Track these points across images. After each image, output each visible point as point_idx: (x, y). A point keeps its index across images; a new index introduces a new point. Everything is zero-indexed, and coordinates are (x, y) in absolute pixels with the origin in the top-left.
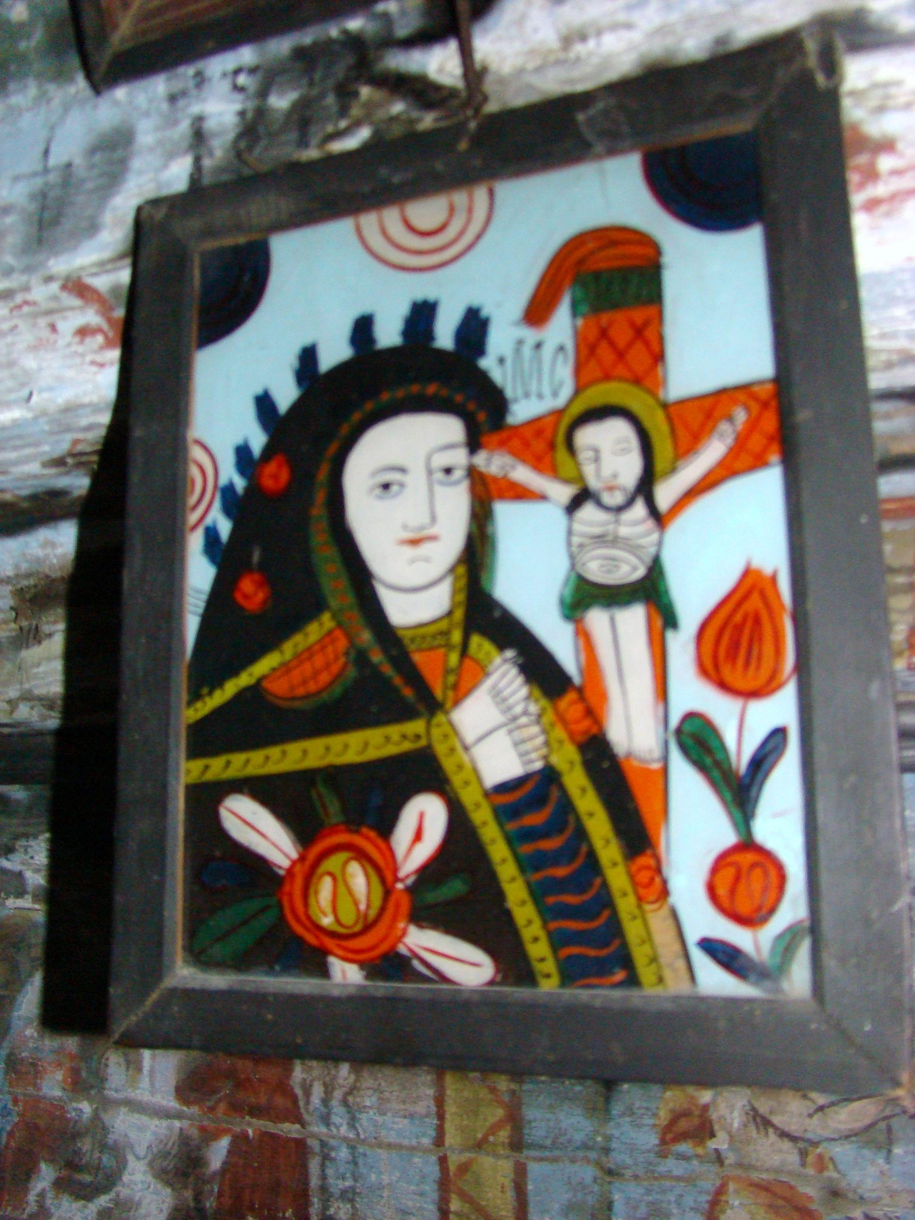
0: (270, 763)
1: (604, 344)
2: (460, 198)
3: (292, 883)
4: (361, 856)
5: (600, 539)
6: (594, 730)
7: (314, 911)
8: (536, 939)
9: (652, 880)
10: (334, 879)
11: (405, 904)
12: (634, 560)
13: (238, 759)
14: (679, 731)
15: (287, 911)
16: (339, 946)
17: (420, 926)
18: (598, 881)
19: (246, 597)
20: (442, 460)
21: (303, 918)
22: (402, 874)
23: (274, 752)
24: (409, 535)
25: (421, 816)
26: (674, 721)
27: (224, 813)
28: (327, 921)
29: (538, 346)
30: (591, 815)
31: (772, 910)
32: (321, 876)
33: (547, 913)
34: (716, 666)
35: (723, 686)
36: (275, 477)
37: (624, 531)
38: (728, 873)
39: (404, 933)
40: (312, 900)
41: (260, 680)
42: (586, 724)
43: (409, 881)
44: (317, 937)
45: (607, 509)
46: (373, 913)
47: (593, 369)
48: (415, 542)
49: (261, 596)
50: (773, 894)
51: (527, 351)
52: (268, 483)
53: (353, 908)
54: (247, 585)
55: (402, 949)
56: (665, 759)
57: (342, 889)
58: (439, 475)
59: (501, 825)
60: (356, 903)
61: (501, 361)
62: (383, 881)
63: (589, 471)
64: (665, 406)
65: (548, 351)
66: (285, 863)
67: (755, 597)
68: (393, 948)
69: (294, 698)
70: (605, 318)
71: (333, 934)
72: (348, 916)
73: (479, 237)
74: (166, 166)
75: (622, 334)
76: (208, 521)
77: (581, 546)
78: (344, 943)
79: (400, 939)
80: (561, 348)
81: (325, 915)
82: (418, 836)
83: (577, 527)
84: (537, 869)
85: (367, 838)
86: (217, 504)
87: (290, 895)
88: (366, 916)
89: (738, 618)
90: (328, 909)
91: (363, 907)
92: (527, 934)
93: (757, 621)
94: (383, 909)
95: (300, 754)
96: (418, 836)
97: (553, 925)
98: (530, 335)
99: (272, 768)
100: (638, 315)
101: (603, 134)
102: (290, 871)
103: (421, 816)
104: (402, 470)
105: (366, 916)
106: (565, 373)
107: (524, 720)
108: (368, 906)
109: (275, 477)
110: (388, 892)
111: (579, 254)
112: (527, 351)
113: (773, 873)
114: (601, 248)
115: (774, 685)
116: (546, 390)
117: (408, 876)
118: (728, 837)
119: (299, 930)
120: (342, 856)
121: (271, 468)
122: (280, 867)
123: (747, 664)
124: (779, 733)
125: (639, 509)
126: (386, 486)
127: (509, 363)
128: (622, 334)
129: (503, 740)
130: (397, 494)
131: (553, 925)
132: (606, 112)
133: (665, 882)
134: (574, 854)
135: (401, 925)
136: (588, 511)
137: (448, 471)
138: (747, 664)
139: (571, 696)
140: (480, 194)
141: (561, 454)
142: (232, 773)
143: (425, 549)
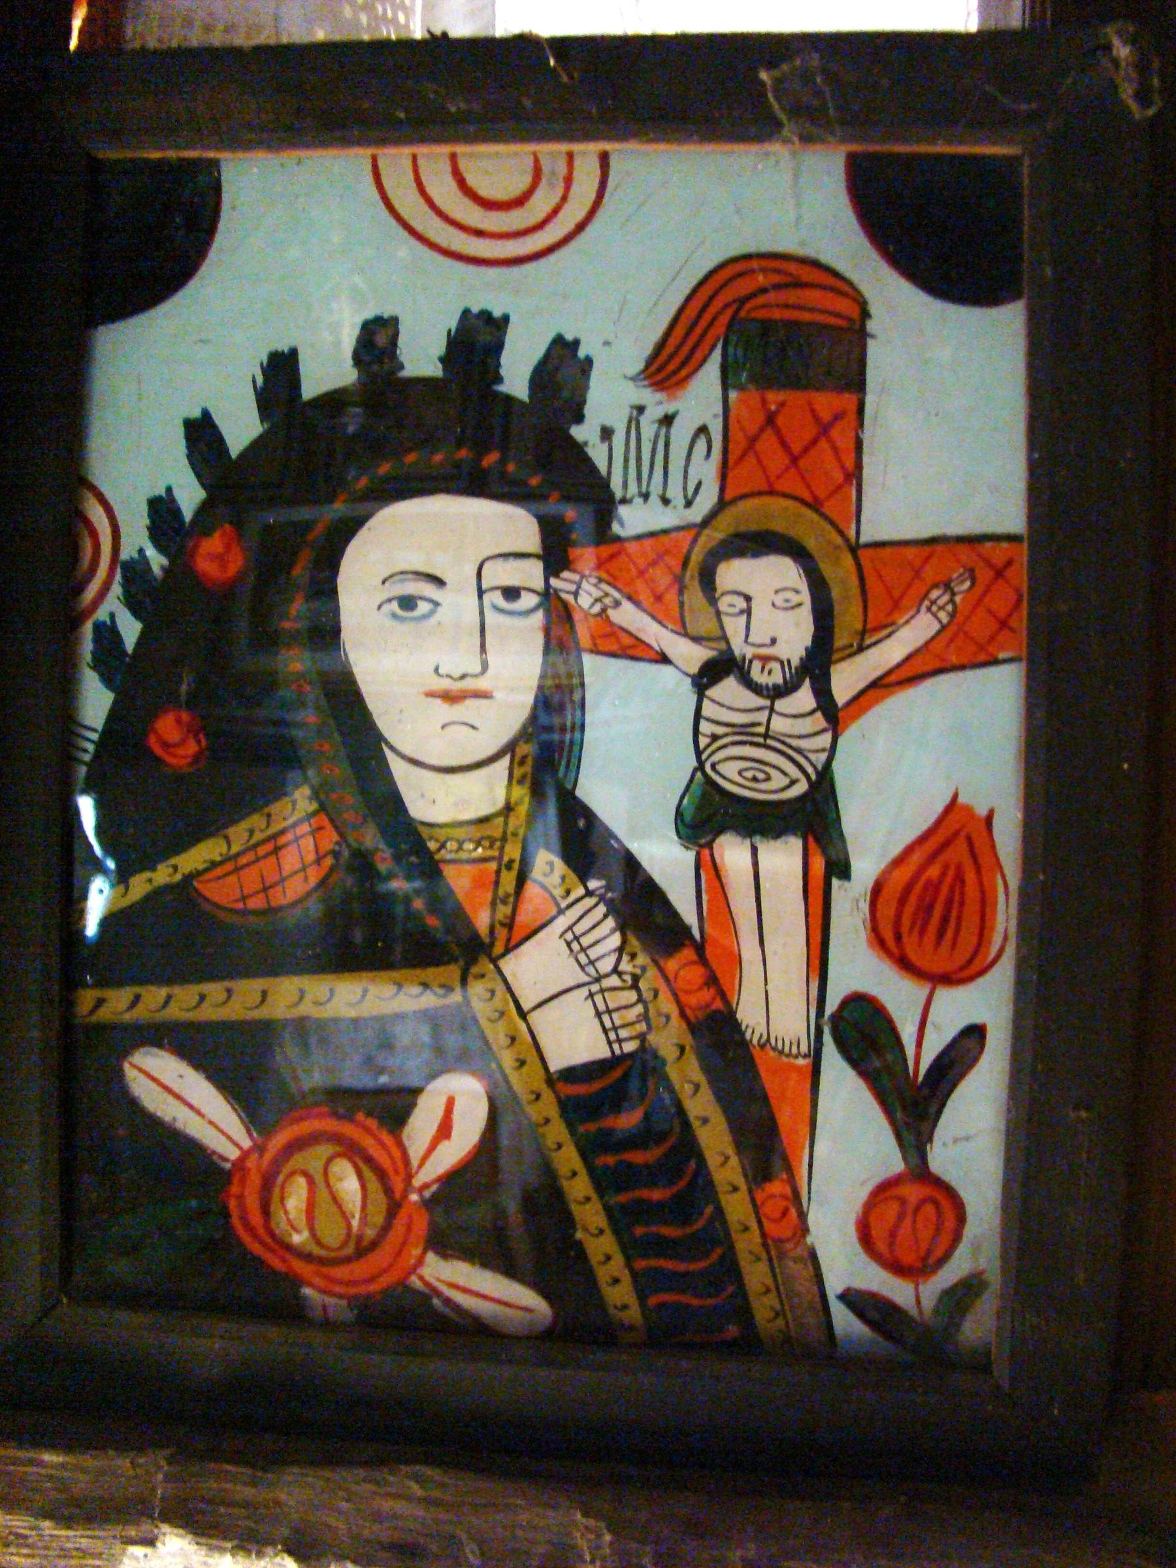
0: (205, 1005)
1: (769, 434)
2: (552, 152)
3: (243, 1182)
4: (352, 1151)
5: (743, 733)
6: (718, 1004)
7: (280, 1223)
8: (616, 1281)
9: (785, 1212)
10: (311, 1182)
11: (421, 1224)
12: (794, 772)
13: (154, 995)
14: (836, 1018)
15: (236, 1221)
16: (318, 1273)
17: (445, 1256)
18: (709, 1210)
19: (166, 745)
20: (501, 574)
21: (261, 1231)
22: (417, 1182)
23: (214, 990)
24: (445, 684)
25: (450, 1104)
26: (831, 1006)
27: (130, 1073)
28: (298, 1239)
29: (668, 420)
30: (705, 1121)
31: (942, 1261)
32: (292, 1174)
33: (630, 1248)
34: (898, 938)
35: (905, 964)
36: (221, 559)
37: (779, 725)
38: (891, 1210)
39: (420, 1261)
40: (275, 1207)
41: (189, 878)
42: (706, 995)
43: (427, 1194)
44: (284, 1261)
45: (756, 689)
46: (370, 1233)
47: (747, 475)
48: (450, 698)
49: (192, 748)
50: (945, 1239)
51: (648, 429)
52: (205, 565)
53: (343, 1224)
54: (168, 727)
55: (415, 1282)
56: (816, 1056)
57: (323, 1194)
58: (497, 598)
59: (571, 1126)
60: (346, 1217)
61: (607, 433)
62: (388, 1191)
63: (734, 628)
64: (854, 549)
65: (681, 433)
66: (233, 1154)
67: (961, 846)
68: (403, 1283)
69: (245, 913)
70: (774, 398)
71: (308, 1257)
72: (332, 1233)
73: (581, 227)
74: (647, 1117)
75: (799, 431)
76: (102, 614)
77: (715, 738)
78: (325, 1270)
79: (414, 1269)
80: (703, 430)
81: (298, 1231)
82: (445, 1130)
83: (708, 709)
84: (620, 1189)
85: (368, 1131)
86: (117, 589)
87: (240, 1197)
88: (360, 1238)
89: (933, 872)
90: (302, 1222)
91: (355, 1223)
92: (603, 1274)
93: (960, 878)
94: (386, 1228)
95: (258, 997)
96: (445, 1130)
97: (640, 1264)
98: (656, 404)
99: (208, 1013)
100: (826, 402)
101: (797, 110)
102: (240, 1164)
103: (450, 1104)
104: (439, 582)
105: (360, 1238)
106: (706, 470)
107: (614, 981)
108: (364, 1220)
109: (221, 559)
110: (394, 1207)
111: (743, 287)
112: (648, 429)
113: (950, 1223)
114: (777, 287)
115: (976, 966)
116: (675, 492)
117: (426, 1186)
118: (894, 1162)
119: (256, 1248)
120: (324, 1151)
121: (213, 544)
122: (225, 1159)
123: (941, 935)
124: (975, 1034)
125: (804, 698)
126: (408, 603)
127: (618, 440)
128: (799, 431)
129: (577, 1008)
130: (426, 616)
131: (640, 1264)
132: (806, 76)
133: (802, 1216)
134: (675, 1173)
135: (416, 1252)
136: (728, 689)
137: (511, 593)
138: (941, 935)
139: (688, 954)
140: (587, 153)
141: (695, 596)
142: (141, 1013)
143: (468, 710)
